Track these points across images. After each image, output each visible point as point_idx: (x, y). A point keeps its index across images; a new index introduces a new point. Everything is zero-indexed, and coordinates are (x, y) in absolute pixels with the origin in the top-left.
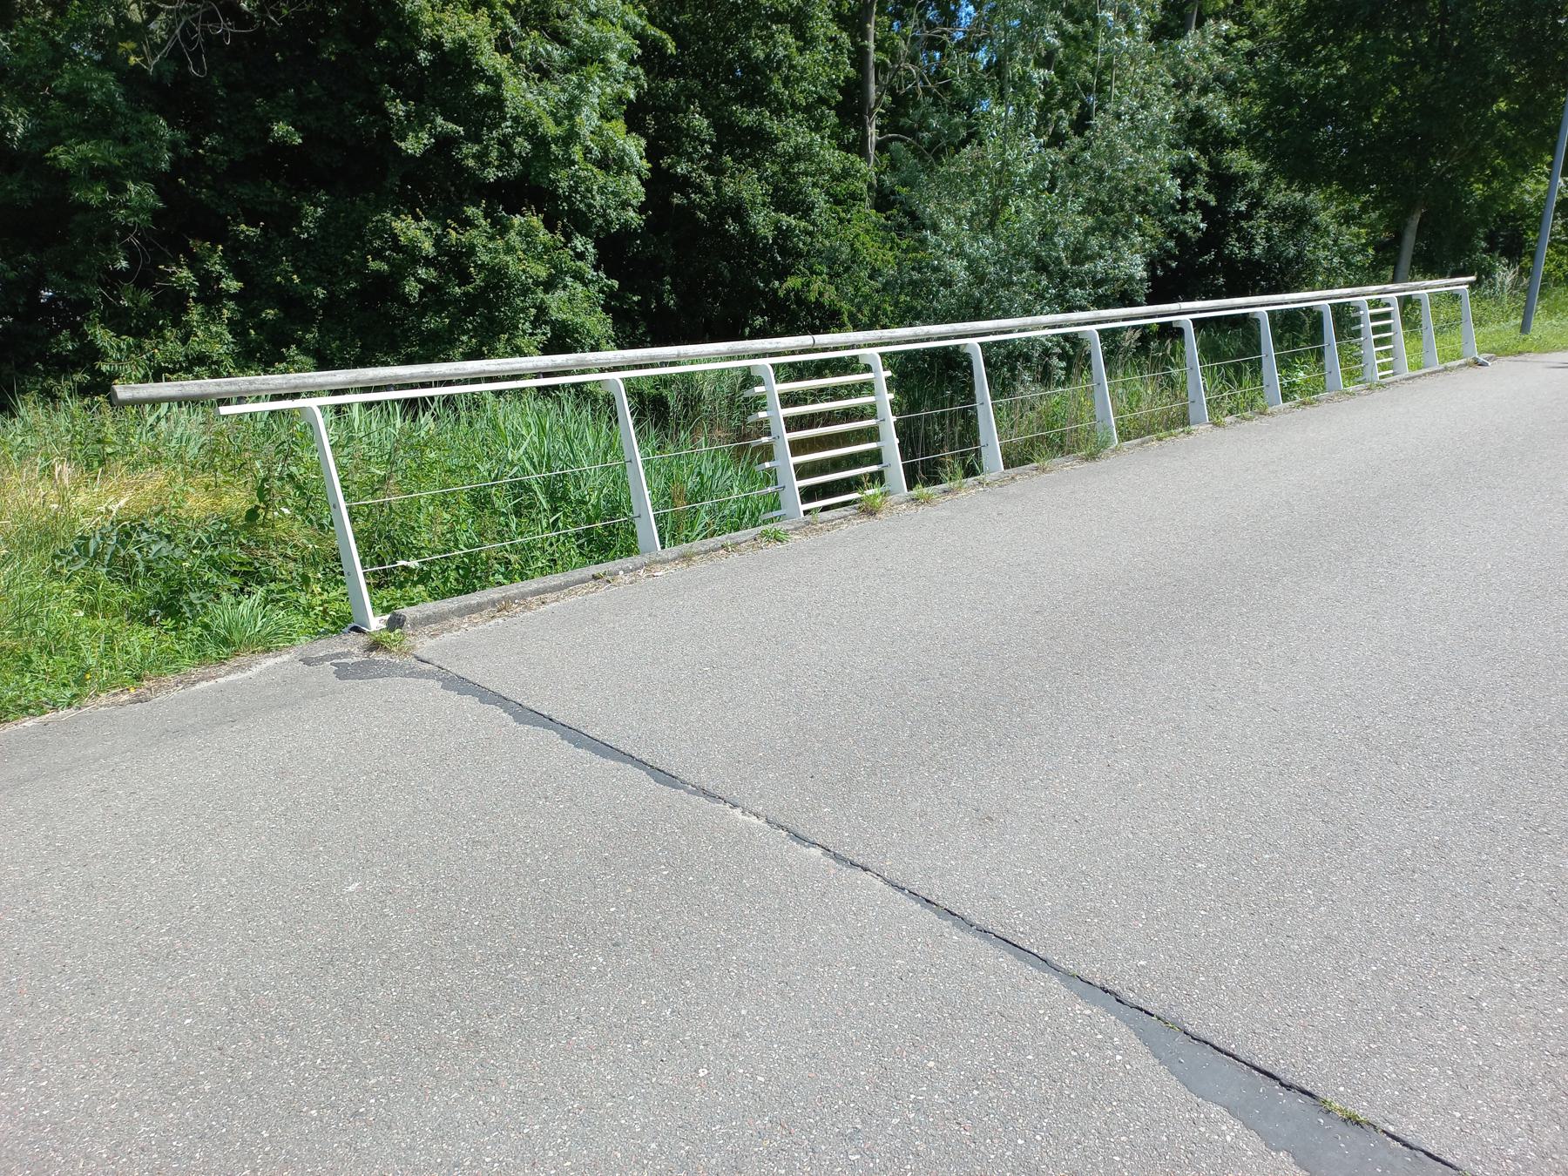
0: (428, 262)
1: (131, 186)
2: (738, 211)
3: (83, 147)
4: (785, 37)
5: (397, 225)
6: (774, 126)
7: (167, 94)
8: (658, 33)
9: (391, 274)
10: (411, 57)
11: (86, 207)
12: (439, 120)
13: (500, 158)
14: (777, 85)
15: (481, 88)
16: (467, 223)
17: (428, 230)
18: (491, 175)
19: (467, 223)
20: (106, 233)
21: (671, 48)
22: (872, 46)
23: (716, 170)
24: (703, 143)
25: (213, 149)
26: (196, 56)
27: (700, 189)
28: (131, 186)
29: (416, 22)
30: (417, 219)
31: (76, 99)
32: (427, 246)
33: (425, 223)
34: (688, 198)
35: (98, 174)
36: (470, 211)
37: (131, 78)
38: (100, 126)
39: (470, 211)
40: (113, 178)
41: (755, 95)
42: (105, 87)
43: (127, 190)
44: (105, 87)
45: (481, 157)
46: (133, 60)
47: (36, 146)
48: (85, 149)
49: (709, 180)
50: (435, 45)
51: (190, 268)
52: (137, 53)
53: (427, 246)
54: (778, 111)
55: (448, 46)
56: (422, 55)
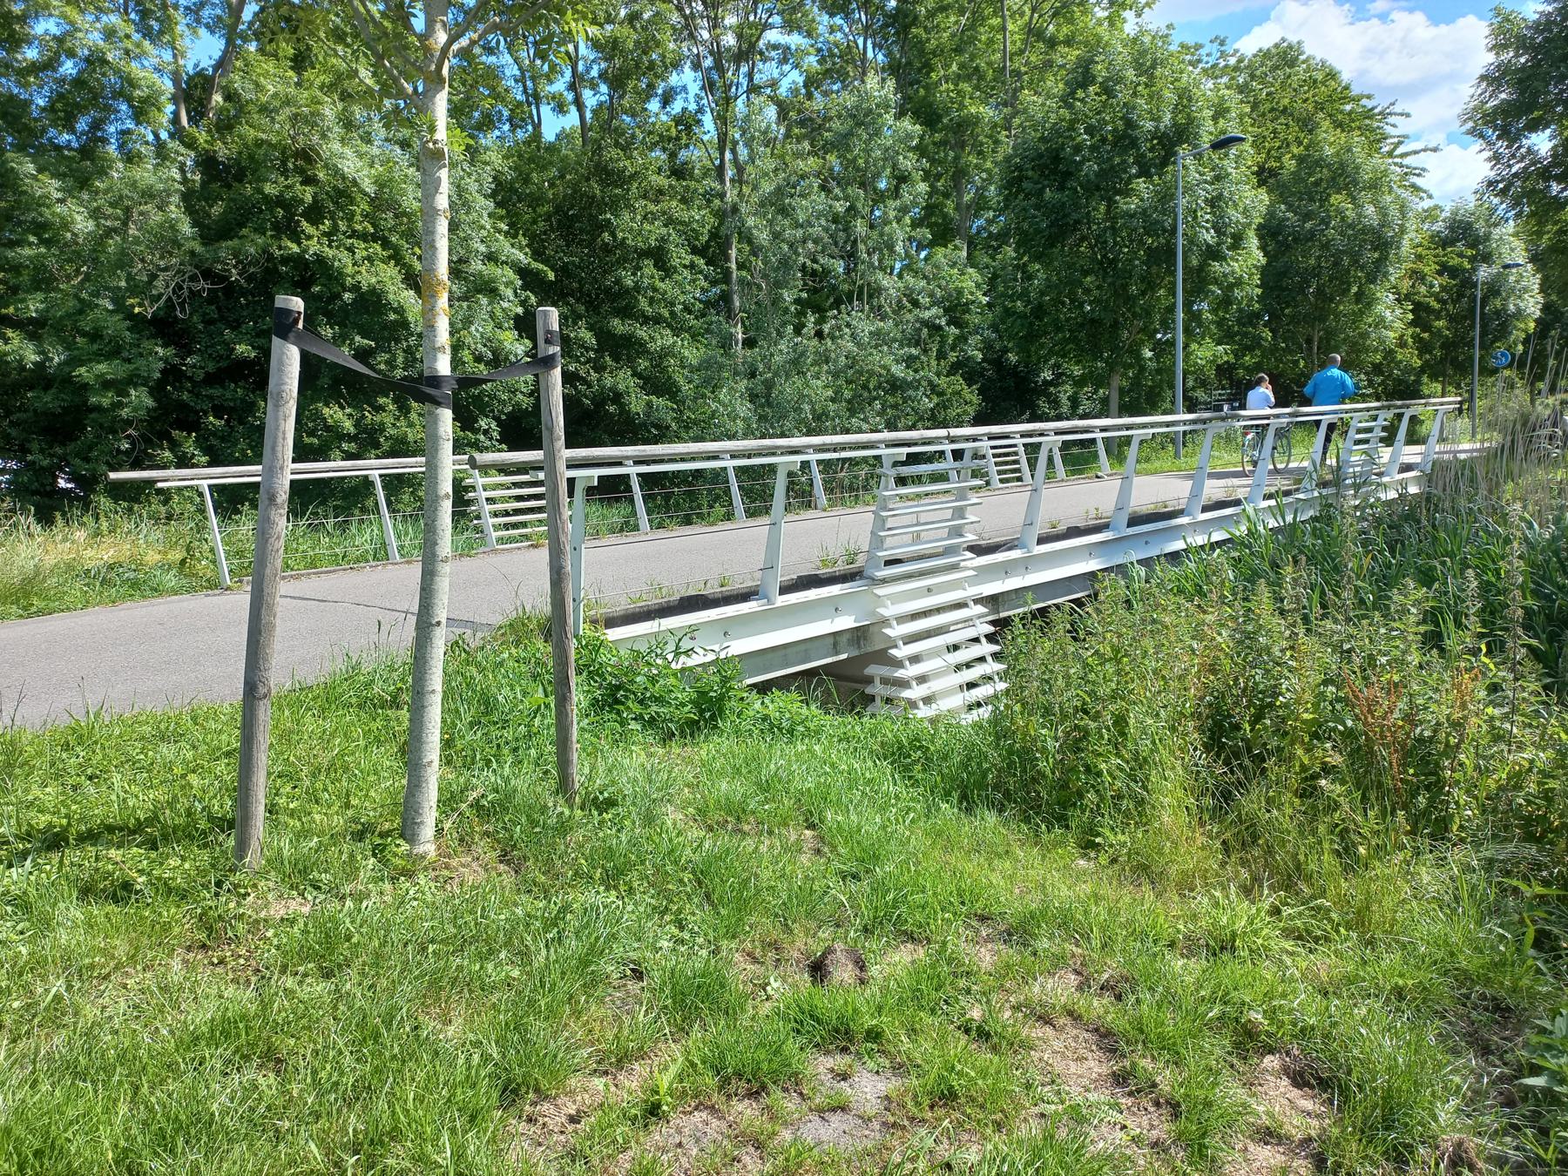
0: (351, 438)
1: (133, 392)
2: (617, 397)
3: (101, 366)
4: (649, 268)
5: (326, 411)
6: (642, 333)
7: (164, 327)
8: (541, 266)
9: (320, 446)
10: (338, 296)
11: (98, 408)
12: (358, 338)
13: (406, 361)
14: (643, 303)
15: (393, 317)
16: (380, 409)
17: (350, 415)
18: (399, 373)
19: (380, 409)
20: (117, 427)
21: (551, 276)
22: (734, 266)
23: (599, 368)
24: (587, 349)
25: (194, 366)
26: (182, 305)
27: (584, 381)
28: (133, 392)
29: (341, 274)
30: (342, 408)
31: (95, 336)
32: (348, 426)
33: (348, 411)
34: (576, 388)
35: (107, 385)
36: (382, 401)
37: (137, 323)
38: (114, 352)
39: (382, 401)
40: (119, 387)
41: (628, 312)
42: (115, 326)
43: (129, 395)
44: (115, 326)
45: (391, 364)
46: (137, 310)
47: (67, 369)
48: (102, 368)
49: (594, 375)
50: (356, 288)
51: (171, 450)
52: (140, 305)
53: (348, 426)
54: (646, 320)
55: (365, 288)
56: (347, 296)
